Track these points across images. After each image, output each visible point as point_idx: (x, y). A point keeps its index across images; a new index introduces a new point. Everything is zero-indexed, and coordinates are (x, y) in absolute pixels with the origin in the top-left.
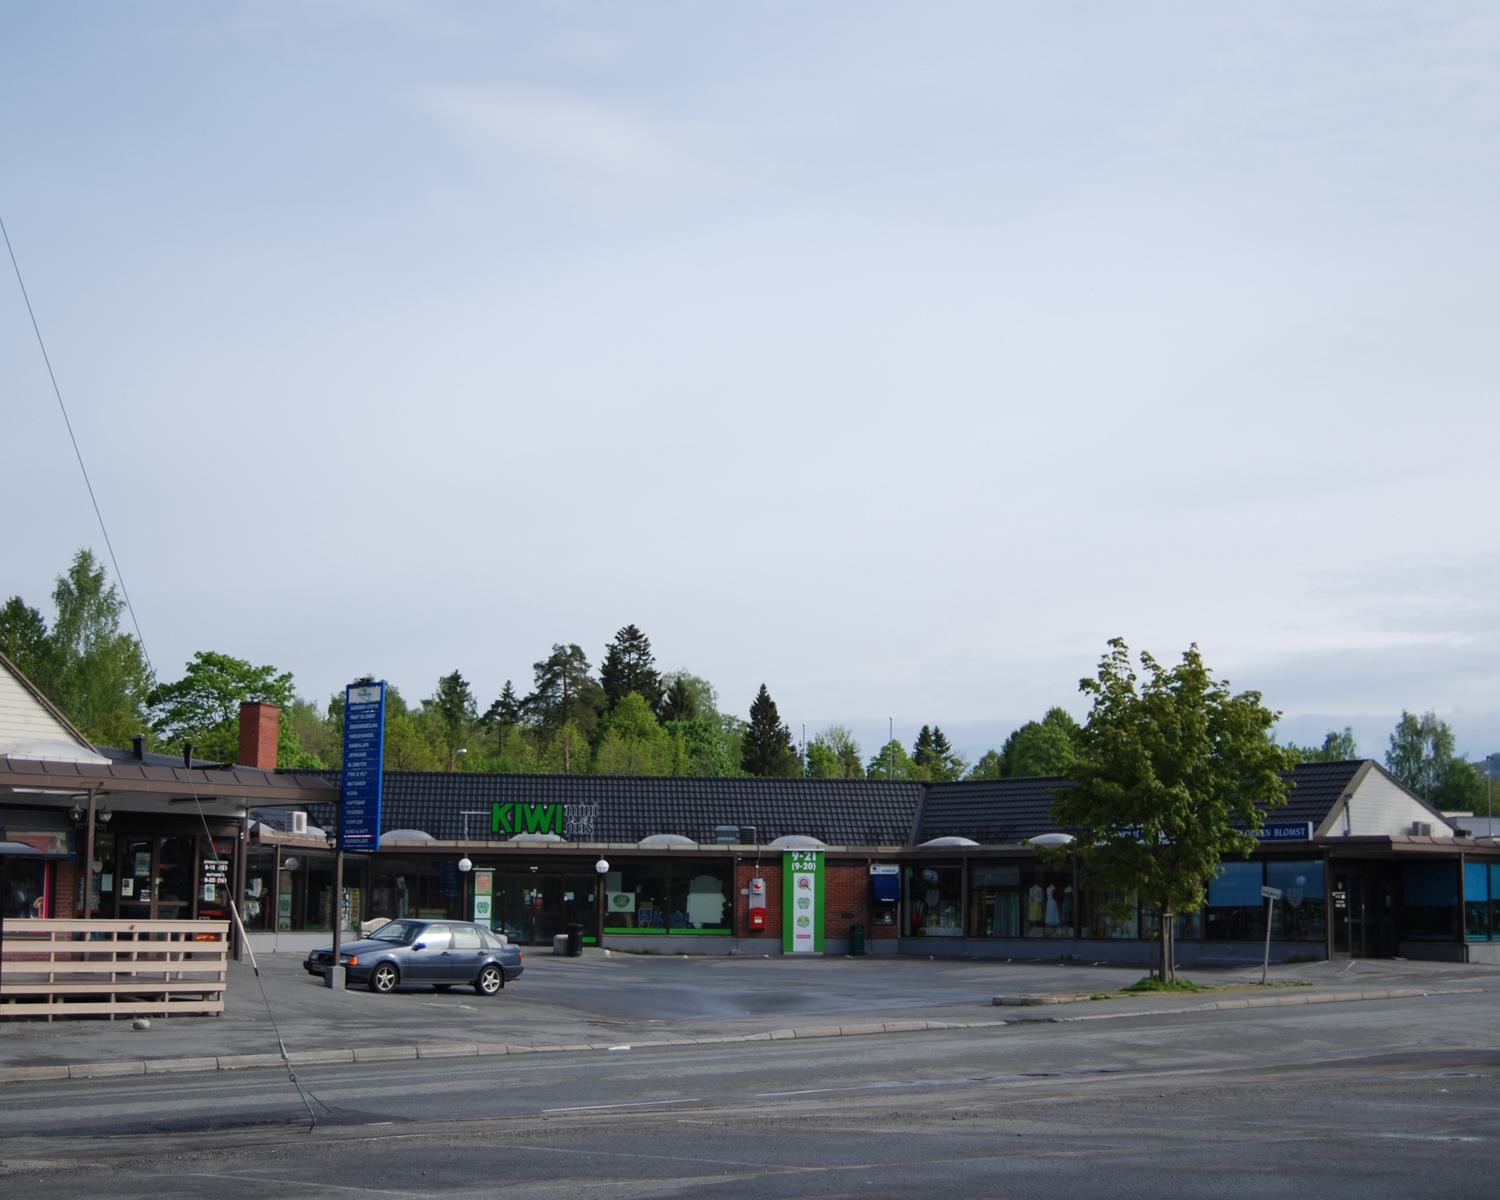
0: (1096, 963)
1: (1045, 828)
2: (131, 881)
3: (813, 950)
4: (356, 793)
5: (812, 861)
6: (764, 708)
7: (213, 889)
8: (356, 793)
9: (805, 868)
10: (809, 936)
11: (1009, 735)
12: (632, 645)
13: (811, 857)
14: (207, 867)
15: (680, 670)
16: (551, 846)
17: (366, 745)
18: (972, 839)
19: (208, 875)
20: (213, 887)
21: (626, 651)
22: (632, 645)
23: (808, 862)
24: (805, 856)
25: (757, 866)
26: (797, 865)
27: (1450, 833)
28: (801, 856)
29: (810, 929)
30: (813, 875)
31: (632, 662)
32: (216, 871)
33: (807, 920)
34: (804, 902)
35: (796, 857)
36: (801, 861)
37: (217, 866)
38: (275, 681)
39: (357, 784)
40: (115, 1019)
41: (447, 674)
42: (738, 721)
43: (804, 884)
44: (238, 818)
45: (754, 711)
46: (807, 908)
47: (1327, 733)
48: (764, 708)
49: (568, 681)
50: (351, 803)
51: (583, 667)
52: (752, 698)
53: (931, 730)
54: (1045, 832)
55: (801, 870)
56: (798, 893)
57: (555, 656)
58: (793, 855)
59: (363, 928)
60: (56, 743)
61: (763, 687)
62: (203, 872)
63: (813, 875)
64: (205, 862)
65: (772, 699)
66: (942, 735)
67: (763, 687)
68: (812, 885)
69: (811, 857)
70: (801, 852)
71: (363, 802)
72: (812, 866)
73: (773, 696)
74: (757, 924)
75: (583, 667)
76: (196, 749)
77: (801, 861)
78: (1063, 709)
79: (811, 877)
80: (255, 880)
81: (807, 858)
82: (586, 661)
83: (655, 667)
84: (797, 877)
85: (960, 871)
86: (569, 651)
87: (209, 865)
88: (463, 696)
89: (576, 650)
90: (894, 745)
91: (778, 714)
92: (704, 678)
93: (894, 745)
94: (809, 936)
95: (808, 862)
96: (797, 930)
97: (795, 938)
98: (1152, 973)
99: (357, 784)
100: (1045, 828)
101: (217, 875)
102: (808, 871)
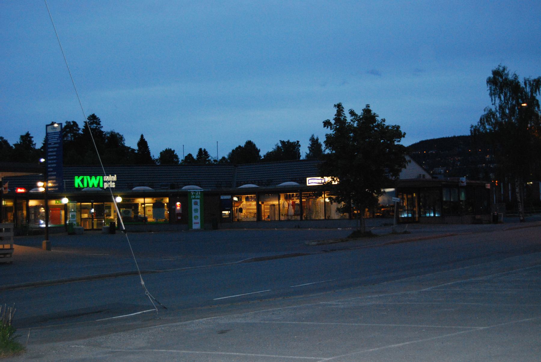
1: (285, 180)
3: (200, 228)
5: (199, 195)
6: (143, 143)
9: (196, 198)
10: (194, 223)
11: (231, 151)
12: (94, 121)
13: (198, 193)
15: (112, 130)
17: (55, 149)
18: (151, 187)
21: (92, 124)
22: (94, 121)
23: (197, 195)
24: (196, 193)
25: (178, 197)
26: (193, 197)
27: (431, 178)
28: (195, 193)
29: (199, 221)
30: (199, 200)
31: (94, 128)
33: (198, 217)
34: (196, 210)
35: (193, 193)
36: (194, 195)
39: (53, 165)
41: (24, 134)
42: (131, 149)
43: (196, 203)
45: (139, 144)
46: (197, 212)
47: (454, 135)
48: (143, 143)
49: (72, 134)
50: (50, 174)
51: (78, 129)
52: (138, 139)
53: (203, 149)
54: (287, 181)
55: (195, 198)
56: (194, 207)
57: (67, 125)
58: (192, 193)
61: (142, 136)
63: (199, 200)
65: (146, 140)
66: (207, 152)
67: (142, 136)
68: (199, 204)
69: (198, 193)
70: (194, 192)
72: (199, 197)
73: (146, 138)
74: (179, 219)
75: (78, 129)
77: (194, 195)
78: (252, 141)
79: (198, 201)
80: (9, 213)
81: (197, 194)
82: (79, 127)
83: (102, 129)
84: (193, 201)
86: (72, 123)
88: (31, 142)
89: (74, 123)
90: (190, 155)
91: (148, 146)
92: (121, 134)
93: (190, 155)
94: (194, 223)
95: (197, 195)
96: (194, 221)
97: (193, 223)
98: (32, 214)
99: (53, 165)
100: (285, 180)
102: (197, 199)
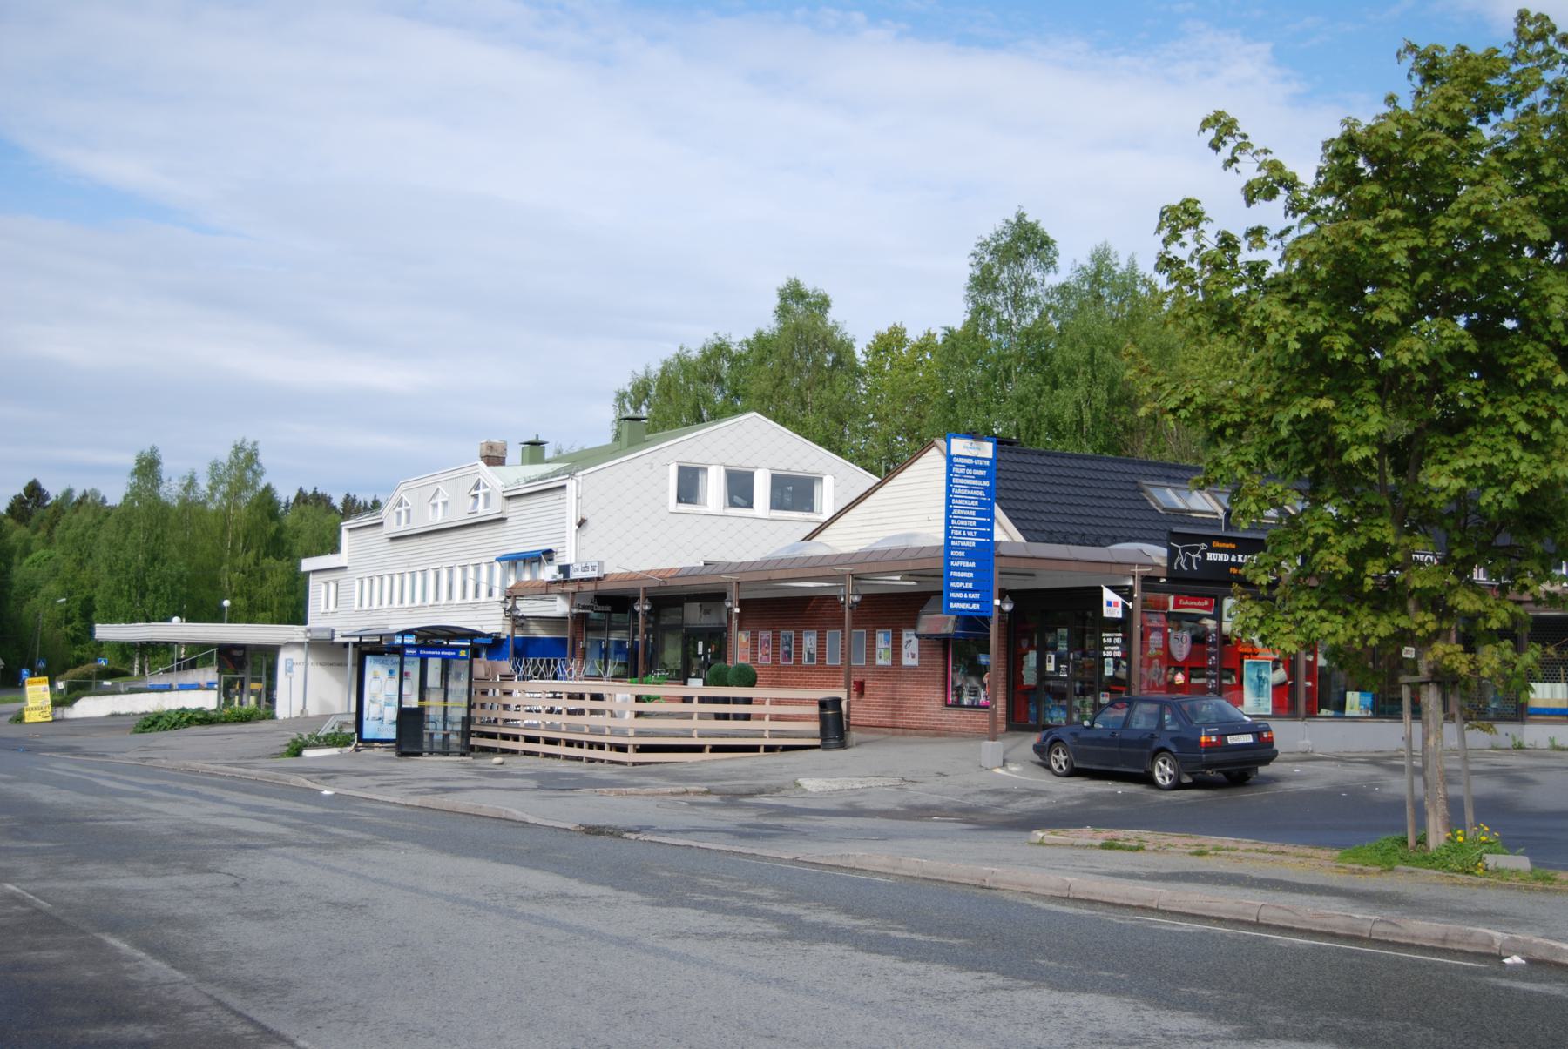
0: (1522, 850)
2: (1053, 657)
4: (962, 554)
7: (1112, 663)
8: (962, 554)
14: (1104, 641)
16: (363, 640)
19: (1106, 648)
20: (1111, 660)
32: (1112, 644)
37: (1113, 638)
38: (1342, 336)
40: (765, 751)
44: (1127, 587)
59: (296, 713)
60: (1000, 525)
62: (1101, 646)
64: (1104, 635)
71: (973, 565)
76: (122, 596)
85: (941, 613)
87: (1106, 638)
101: (1113, 648)
